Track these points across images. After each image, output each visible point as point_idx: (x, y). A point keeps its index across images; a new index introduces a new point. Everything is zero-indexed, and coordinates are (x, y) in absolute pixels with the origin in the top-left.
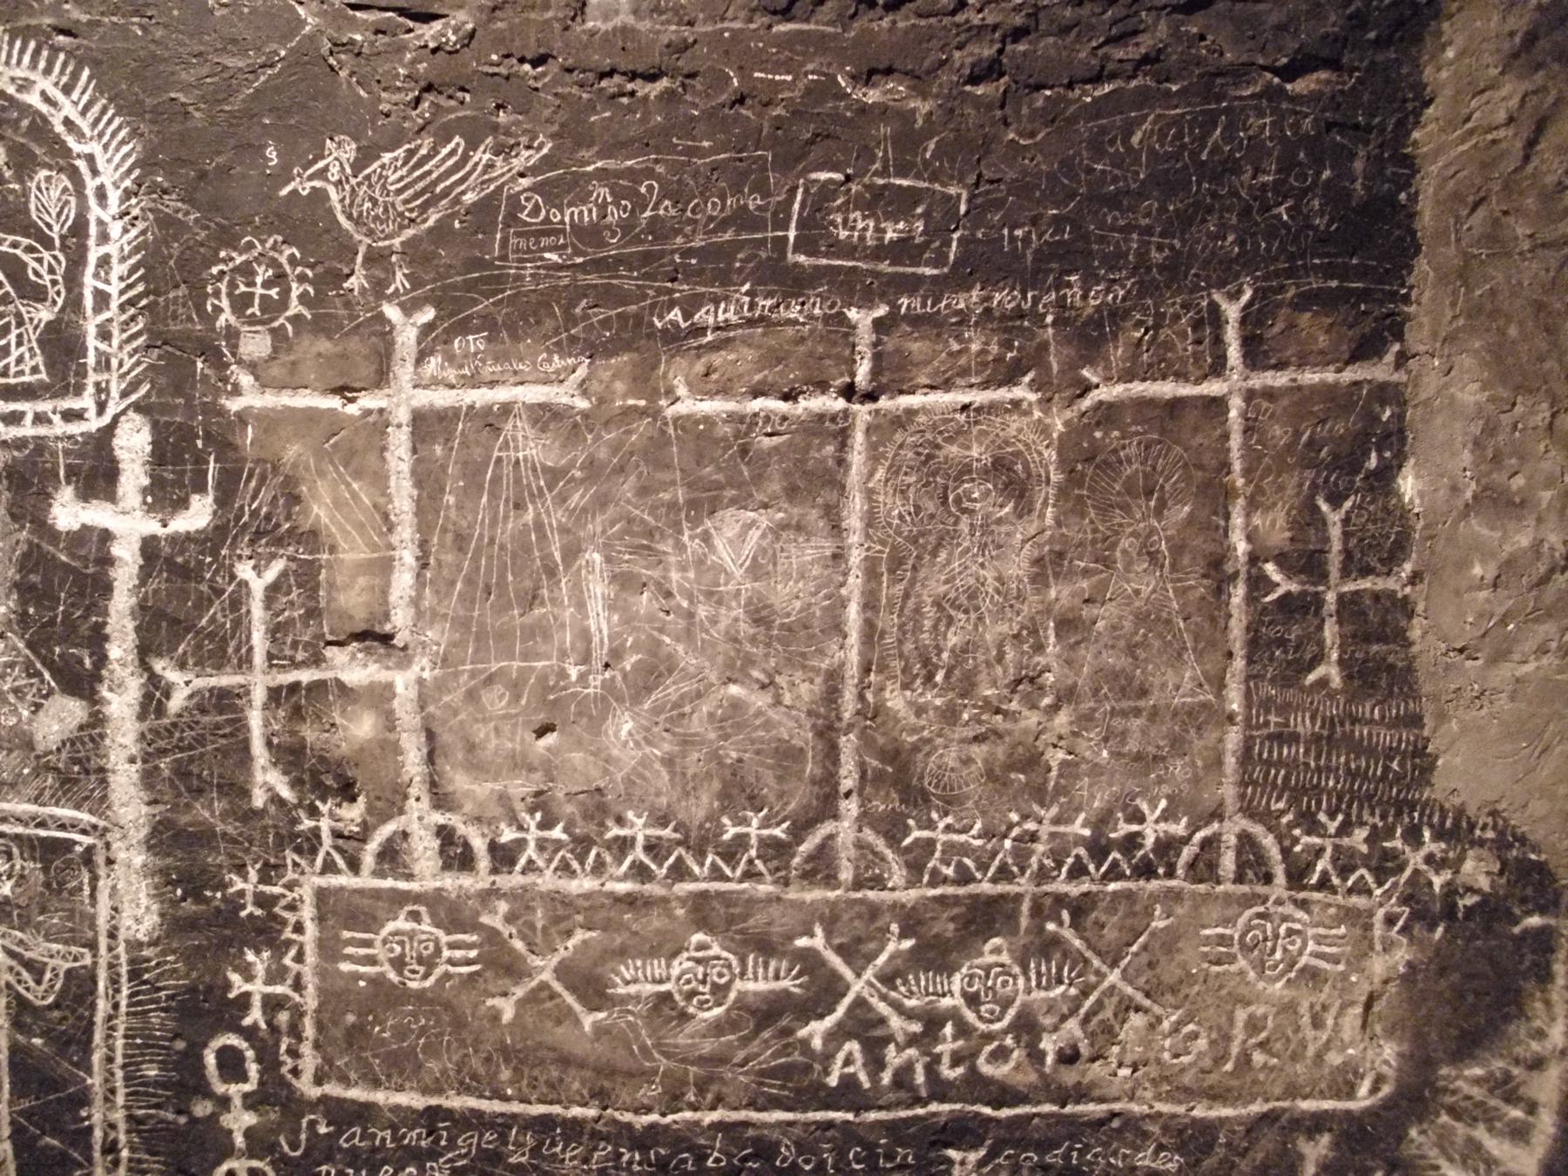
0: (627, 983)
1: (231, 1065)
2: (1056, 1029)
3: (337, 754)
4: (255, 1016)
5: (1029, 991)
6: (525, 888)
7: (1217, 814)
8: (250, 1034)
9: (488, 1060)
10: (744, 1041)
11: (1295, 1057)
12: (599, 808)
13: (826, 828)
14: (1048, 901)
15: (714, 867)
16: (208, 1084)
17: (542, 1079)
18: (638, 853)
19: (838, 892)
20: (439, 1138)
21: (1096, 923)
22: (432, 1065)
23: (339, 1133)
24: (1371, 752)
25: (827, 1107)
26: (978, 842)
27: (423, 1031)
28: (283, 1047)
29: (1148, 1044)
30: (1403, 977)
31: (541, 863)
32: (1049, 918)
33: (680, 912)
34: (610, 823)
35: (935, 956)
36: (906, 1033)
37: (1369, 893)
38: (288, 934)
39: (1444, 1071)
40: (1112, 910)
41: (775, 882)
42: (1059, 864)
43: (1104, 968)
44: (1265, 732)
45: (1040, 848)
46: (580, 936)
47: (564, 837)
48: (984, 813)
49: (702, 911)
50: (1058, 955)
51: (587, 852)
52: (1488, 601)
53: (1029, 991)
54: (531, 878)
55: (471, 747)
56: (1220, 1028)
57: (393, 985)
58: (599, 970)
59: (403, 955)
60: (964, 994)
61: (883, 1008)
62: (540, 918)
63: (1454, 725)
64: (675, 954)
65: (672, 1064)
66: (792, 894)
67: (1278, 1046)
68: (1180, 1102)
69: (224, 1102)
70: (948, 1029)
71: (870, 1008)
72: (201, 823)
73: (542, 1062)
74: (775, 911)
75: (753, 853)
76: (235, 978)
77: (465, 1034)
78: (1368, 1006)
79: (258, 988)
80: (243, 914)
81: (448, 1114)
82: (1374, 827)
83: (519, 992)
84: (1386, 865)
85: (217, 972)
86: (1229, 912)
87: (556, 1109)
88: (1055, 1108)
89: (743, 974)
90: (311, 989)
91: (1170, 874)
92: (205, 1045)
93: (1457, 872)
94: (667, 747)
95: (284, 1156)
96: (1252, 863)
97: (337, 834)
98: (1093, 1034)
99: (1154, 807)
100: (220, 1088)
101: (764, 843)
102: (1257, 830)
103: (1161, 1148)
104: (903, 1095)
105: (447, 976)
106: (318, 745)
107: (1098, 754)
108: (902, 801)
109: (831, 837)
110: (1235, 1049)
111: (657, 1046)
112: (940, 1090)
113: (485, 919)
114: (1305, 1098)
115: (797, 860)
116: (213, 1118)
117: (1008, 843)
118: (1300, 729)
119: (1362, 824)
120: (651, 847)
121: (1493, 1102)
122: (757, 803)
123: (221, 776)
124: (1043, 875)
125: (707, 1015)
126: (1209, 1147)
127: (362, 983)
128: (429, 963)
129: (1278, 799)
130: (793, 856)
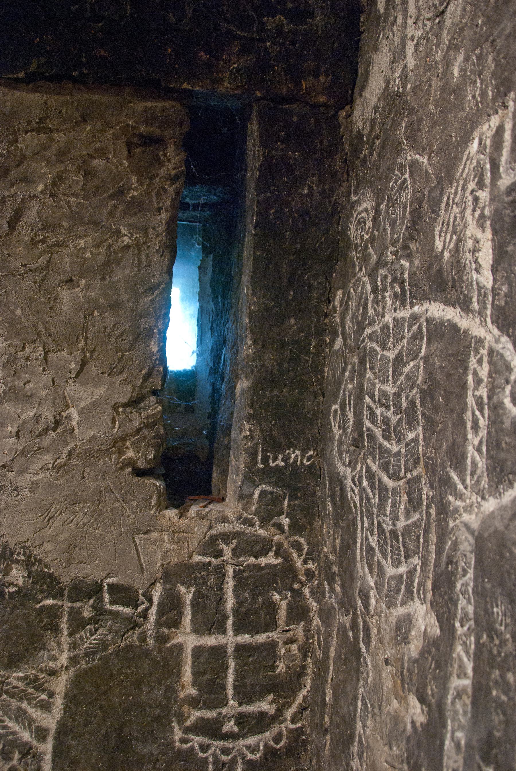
52: (13, 443)
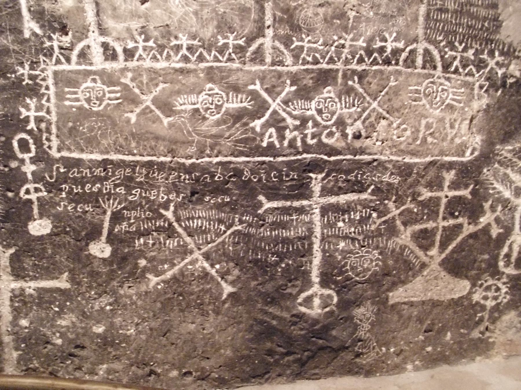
0: (181, 105)
1: (24, 146)
3: (58, 13)
4: (32, 125)
5: (342, 109)
6: (138, 67)
7: (415, 40)
8: (30, 132)
9: (126, 139)
10: (229, 128)
11: (443, 140)
12: (167, 32)
13: (260, 41)
14: (349, 72)
15: (215, 57)
16: (15, 154)
17: (148, 146)
18: (184, 51)
19: (266, 67)
20: (108, 172)
21: (368, 82)
22: (104, 142)
23: (69, 171)
24: (477, 18)
25: (262, 155)
26: (322, 47)
27: (99, 128)
28: (44, 138)
29: (388, 132)
30: (485, 110)
31: (144, 56)
32: (349, 79)
33: (202, 75)
34: (172, 39)
35: (304, 94)
36: (293, 125)
37: (473, 75)
38: (43, 91)
39: (498, 147)
40: (374, 77)
41: (240, 63)
42: (354, 57)
43: (371, 101)
44: (435, 7)
45: (346, 51)
46: (161, 86)
47: (154, 45)
48: (323, 36)
49: (211, 75)
50: (353, 95)
51: (163, 51)
53: (342, 109)
54: (141, 62)
55: (115, 9)
56: (415, 127)
57: (86, 109)
58: (170, 100)
59: (90, 97)
60: (317, 110)
61: (284, 115)
62: (145, 79)
63: (511, 9)
64: (200, 92)
66: (247, 68)
67: (437, 135)
68: (400, 156)
69: (22, 161)
70: (310, 124)
71: (279, 114)
72: (3, 46)
74: (240, 74)
75: (231, 50)
76: (23, 110)
77: (116, 128)
78: (471, 121)
79: (32, 114)
80: (24, 83)
81: (111, 162)
82: (477, 49)
83: (138, 110)
84: (480, 65)
85: (16, 108)
86: (420, 81)
87: (154, 158)
88: (352, 157)
89: (228, 101)
90: (54, 114)
91: (397, 64)
92: (12, 138)
93: (507, 69)
94: (195, 7)
95: (48, 182)
96: (429, 61)
97: (61, 48)
98: (367, 127)
99: (391, 36)
100: (20, 156)
101: (236, 47)
102: (431, 48)
103: (392, 174)
104: (292, 150)
105: (109, 105)
106: (50, 10)
107: (369, 13)
108: (290, 30)
109: (262, 44)
110: (421, 135)
111: (194, 131)
112: (307, 149)
113: (123, 80)
114: (446, 156)
115: (248, 54)
116: (19, 168)
117: (333, 48)
118: (449, 7)
119: (472, 47)
120: (189, 49)
121: (514, 160)
122: (232, 30)
123: (10, 25)
124: (347, 62)
125: (212, 118)
126: (410, 174)
127: (74, 109)
128: (100, 100)
129: (439, 36)
130: (247, 52)
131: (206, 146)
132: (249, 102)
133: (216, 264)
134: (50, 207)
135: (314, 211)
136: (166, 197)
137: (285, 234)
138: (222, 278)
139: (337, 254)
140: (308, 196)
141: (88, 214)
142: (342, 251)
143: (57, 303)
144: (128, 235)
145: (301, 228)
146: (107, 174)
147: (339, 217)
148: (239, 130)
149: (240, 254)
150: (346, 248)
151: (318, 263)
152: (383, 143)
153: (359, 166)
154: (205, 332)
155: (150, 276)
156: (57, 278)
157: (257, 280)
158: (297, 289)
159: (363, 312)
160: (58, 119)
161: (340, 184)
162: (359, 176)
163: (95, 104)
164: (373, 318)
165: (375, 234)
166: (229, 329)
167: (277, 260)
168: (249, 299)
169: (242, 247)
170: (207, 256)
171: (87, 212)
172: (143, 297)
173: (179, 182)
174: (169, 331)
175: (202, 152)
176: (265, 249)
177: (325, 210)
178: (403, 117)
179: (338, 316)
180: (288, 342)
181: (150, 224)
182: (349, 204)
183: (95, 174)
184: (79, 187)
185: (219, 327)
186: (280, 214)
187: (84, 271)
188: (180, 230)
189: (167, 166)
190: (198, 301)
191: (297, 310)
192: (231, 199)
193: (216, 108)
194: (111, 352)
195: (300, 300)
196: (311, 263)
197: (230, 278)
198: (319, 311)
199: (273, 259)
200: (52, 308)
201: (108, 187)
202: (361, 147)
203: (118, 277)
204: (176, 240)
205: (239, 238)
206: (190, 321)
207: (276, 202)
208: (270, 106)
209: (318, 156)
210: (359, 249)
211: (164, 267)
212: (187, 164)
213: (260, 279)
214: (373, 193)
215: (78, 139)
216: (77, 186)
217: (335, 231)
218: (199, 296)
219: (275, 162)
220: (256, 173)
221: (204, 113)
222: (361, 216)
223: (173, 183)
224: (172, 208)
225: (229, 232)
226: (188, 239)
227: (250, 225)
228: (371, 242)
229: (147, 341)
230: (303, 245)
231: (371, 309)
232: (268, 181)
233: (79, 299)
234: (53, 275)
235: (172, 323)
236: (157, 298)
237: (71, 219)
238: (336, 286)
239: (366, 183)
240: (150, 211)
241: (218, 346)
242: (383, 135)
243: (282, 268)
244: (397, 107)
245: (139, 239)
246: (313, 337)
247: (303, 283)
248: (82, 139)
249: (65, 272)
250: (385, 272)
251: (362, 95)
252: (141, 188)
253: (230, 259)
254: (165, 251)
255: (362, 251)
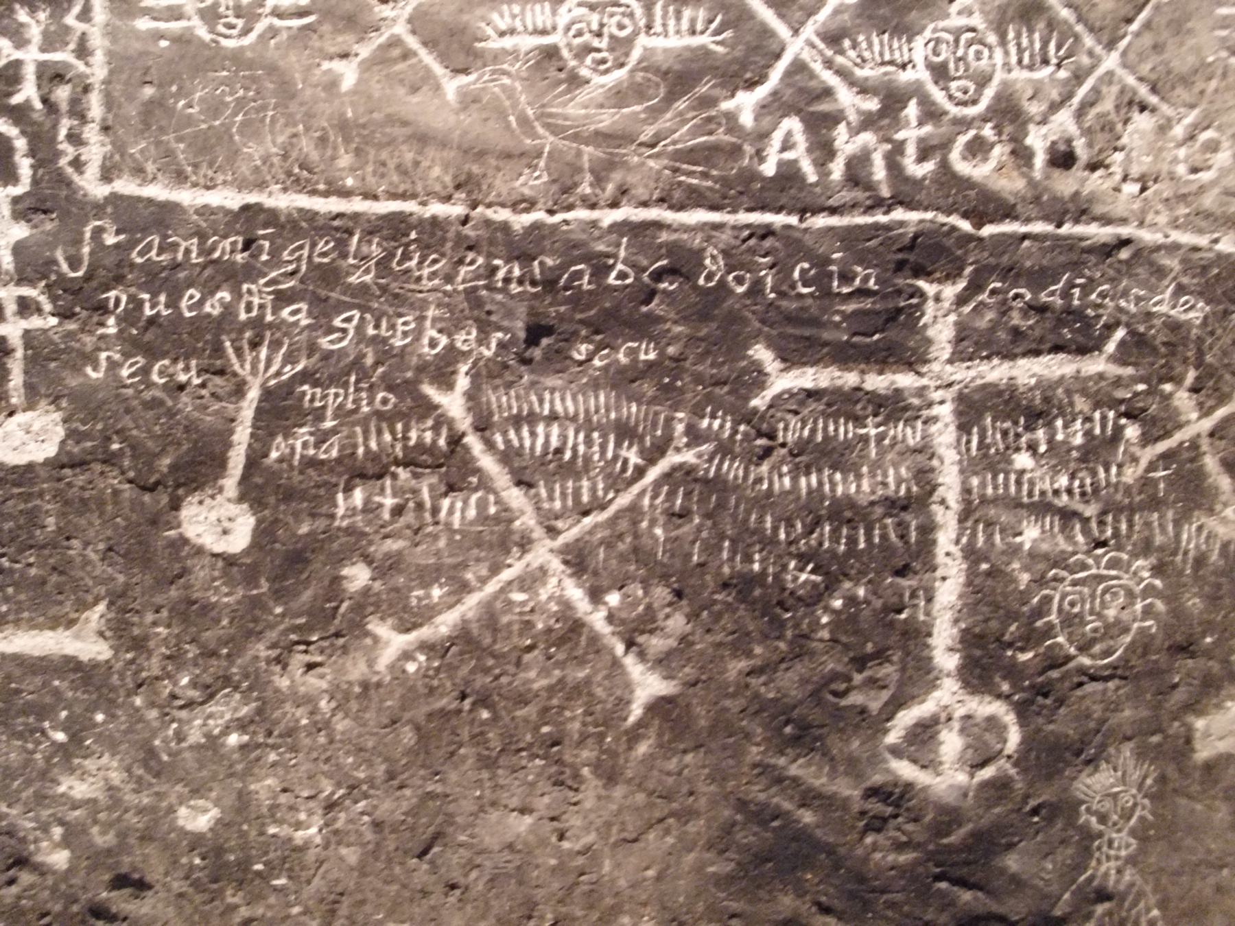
0: (502, 34)
2: (1044, 122)
4: (28, 92)
5: (1007, 67)
10: (655, 113)
17: (392, 164)
23: (131, 244)
25: (763, 208)
27: (240, 103)
28: (63, 132)
29: (1157, 152)
36: (859, 112)
50: (1041, 25)
58: (465, 17)
60: (931, 67)
65: (563, 144)
68: (1201, 231)
70: (912, 110)
71: (812, 75)
73: (391, 142)
77: (293, 107)
81: (271, 217)
83: (364, 51)
87: (409, 206)
88: (1048, 228)
89: (649, 27)
90: (99, 58)
103: (1181, 290)
104: (859, 195)
105: (273, 32)
112: (906, 193)
125: (598, 80)
127: (164, 43)
131: (579, 170)
132: (717, 32)
133: (608, 590)
134: (65, 365)
135: (936, 410)
136: (444, 341)
137: (842, 486)
138: (630, 644)
139: (1016, 565)
140: (912, 357)
141: (184, 398)
142: (1033, 555)
143: (64, 714)
144: (311, 472)
145: (896, 466)
146: (255, 256)
147: (1018, 436)
148: (684, 122)
149: (690, 555)
150: (1045, 547)
151: (953, 598)
152: (1143, 190)
153: (1075, 257)
154: (566, 845)
155: (381, 629)
156: (71, 623)
157: (749, 654)
158: (885, 695)
159: (1109, 786)
160: (111, 72)
161: (1016, 319)
162: (1077, 291)
163: (231, 26)
164: (1144, 811)
165: (1138, 499)
166: (651, 836)
167: (815, 585)
168: (722, 725)
169: (699, 529)
170: (577, 560)
171: (181, 387)
172: (354, 706)
173: (487, 287)
174: (437, 837)
175: (567, 190)
176: (773, 541)
177: (973, 408)
178: (1203, 106)
179: (1026, 797)
180: (852, 896)
181: (387, 437)
182: (1046, 387)
183: (216, 255)
184: (162, 298)
185: (615, 829)
186: (827, 416)
187: (159, 599)
188: (487, 462)
189: (451, 235)
190: (545, 729)
191: (888, 771)
192: (662, 354)
193: (611, 49)
194: (235, 907)
195: (892, 738)
196: (929, 600)
197: (656, 644)
198: (962, 778)
199: (803, 577)
200: (43, 732)
201: (256, 301)
202: (1077, 194)
203: (271, 627)
204: (474, 498)
205: (688, 495)
206: (515, 802)
207: (810, 371)
208: (783, 49)
209: (942, 218)
210: (1088, 553)
211: (428, 596)
212: (517, 227)
213: (758, 650)
214: (1121, 357)
215: (169, 138)
216: (155, 295)
217: (1006, 486)
218: (546, 710)
219: (806, 230)
220: (741, 266)
221: (573, 63)
222: (1088, 434)
223: (471, 293)
224: (463, 382)
225: (653, 474)
226: (515, 497)
227: (724, 450)
228: (1124, 526)
229: (362, 870)
230: (902, 526)
231: (1136, 776)
232: (782, 295)
233: (138, 701)
234: (54, 611)
235: (451, 808)
236: (403, 708)
237: (128, 411)
238: (1016, 687)
239: (1099, 317)
240: (390, 388)
241: (609, 901)
242: (1143, 164)
243: (835, 612)
244: (1185, 69)
245: (348, 490)
246: (938, 878)
247: (903, 670)
248: (180, 139)
249: (96, 602)
250: (1179, 638)
251: (1070, 27)
252: (364, 309)
253: (656, 573)
254: (435, 537)
255: (1097, 559)
